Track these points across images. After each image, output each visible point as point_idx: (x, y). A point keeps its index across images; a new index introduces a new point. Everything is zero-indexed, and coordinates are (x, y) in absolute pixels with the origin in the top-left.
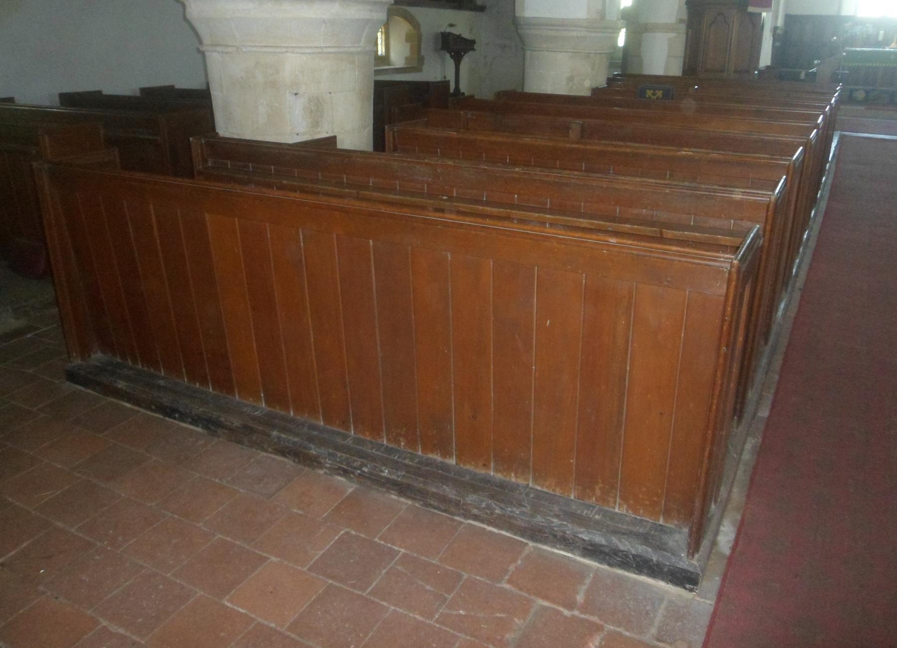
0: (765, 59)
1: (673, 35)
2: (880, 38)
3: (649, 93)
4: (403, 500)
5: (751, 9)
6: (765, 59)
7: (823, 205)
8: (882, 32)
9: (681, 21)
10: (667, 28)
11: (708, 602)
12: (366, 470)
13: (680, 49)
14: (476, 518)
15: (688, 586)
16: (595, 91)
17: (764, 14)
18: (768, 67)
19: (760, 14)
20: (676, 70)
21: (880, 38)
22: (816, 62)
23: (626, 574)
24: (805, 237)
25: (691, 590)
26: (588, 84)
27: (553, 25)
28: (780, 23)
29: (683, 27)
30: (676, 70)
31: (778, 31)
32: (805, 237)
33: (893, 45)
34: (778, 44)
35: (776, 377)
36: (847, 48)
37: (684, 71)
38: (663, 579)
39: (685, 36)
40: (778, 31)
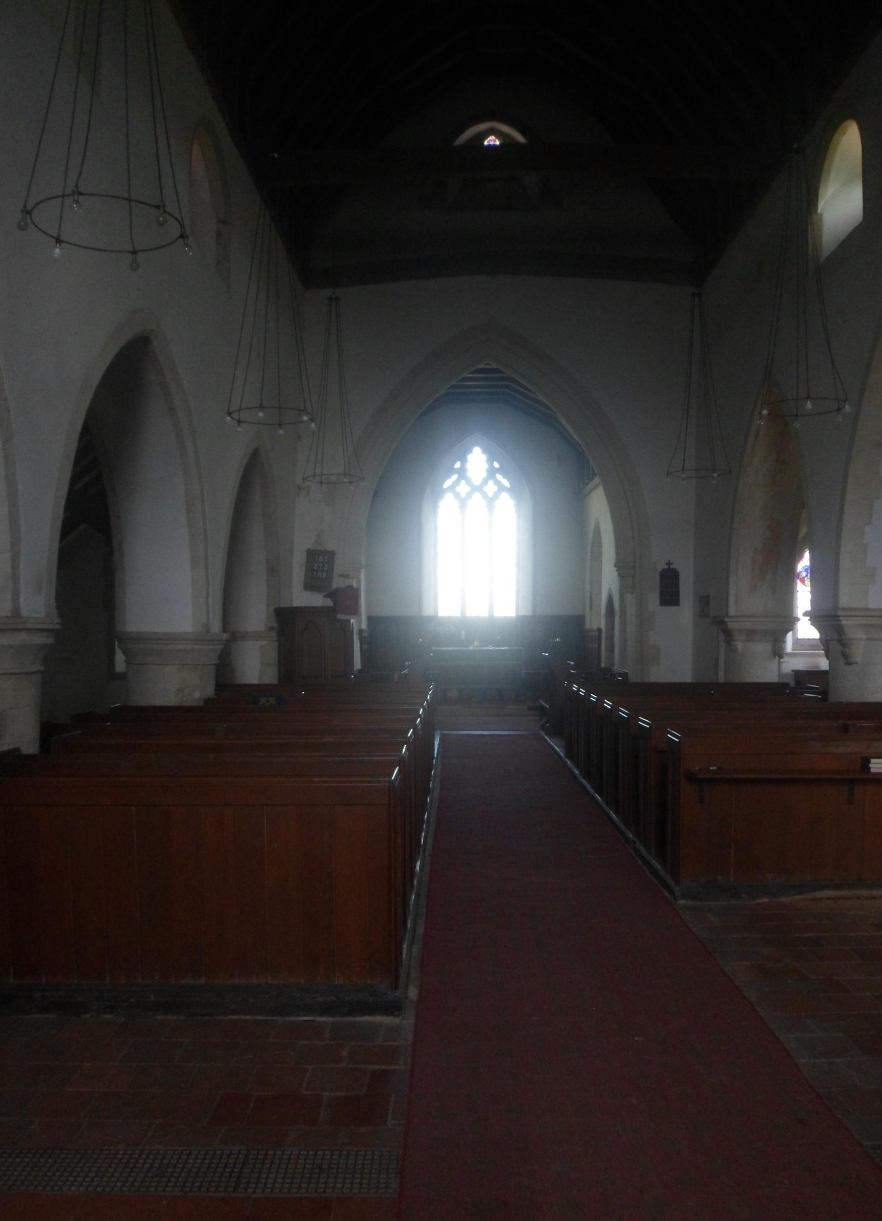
0: (357, 664)
1: (264, 643)
2: (463, 637)
3: (263, 700)
4: (169, 1017)
5: (340, 617)
6: (357, 664)
7: (436, 793)
8: (463, 631)
9: (271, 629)
10: (257, 636)
11: (411, 1021)
12: (132, 1000)
13: (273, 656)
14: (234, 1012)
15: (396, 1013)
16: (207, 701)
17: (352, 621)
18: (359, 670)
19: (349, 621)
20: (271, 677)
21: (463, 637)
22: (407, 663)
23: (354, 1019)
24: (418, 868)
25: (399, 1016)
26: (197, 695)
27: (162, 639)
28: (364, 626)
29: (274, 634)
30: (271, 677)
31: (365, 634)
32: (418, 868)
33: (476, 643)
34: (365, 647)
35: (424, 910)
36: (433, 648)
37: (280, 679)
38: (378, 1014)
39: (277, 643)
40: (365, 634)
